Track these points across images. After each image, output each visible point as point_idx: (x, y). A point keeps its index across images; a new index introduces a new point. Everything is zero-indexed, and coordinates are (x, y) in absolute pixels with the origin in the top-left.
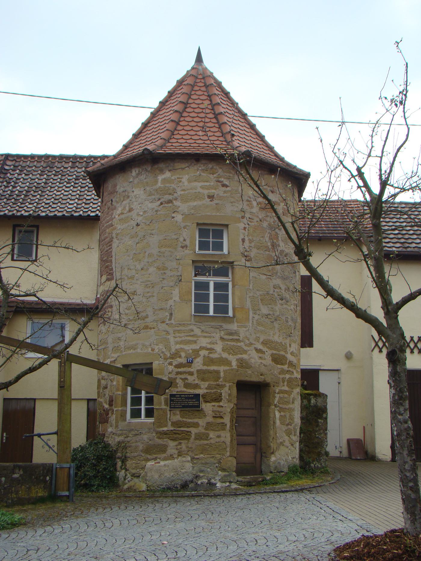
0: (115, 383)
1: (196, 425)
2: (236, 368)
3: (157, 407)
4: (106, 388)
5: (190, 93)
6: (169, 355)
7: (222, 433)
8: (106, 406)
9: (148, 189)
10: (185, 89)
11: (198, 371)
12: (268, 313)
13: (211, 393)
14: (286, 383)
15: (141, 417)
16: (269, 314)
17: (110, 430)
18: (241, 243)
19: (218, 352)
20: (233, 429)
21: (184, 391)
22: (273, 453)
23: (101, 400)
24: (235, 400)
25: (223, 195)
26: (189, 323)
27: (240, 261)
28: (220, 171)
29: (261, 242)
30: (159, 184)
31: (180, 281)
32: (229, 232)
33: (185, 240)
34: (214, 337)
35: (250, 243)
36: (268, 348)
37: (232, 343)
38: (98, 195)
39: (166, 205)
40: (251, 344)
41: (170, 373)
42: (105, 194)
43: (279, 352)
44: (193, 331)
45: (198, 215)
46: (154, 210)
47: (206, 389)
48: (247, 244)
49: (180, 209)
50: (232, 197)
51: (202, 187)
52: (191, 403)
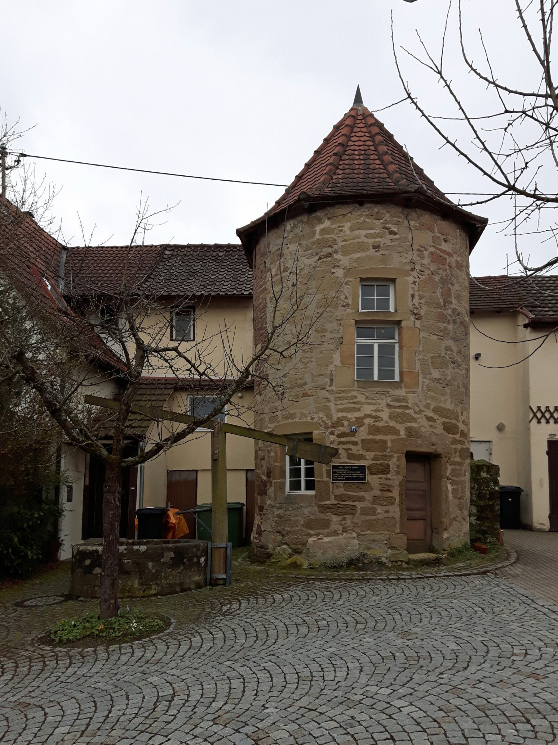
0: (272, 454)
1: (362, 499)
2: (405, 437)
3: (319, 479)
4: (263, 459)
5: (350, 135)
6: (330, 424)
7: (390, 508)
8: (264, 478)
9: (304, 242)
10: (344, 131)
11: (362, 440)
12: (439, 377)
13: (377, 464)
14: (458, 454)
15: (300, 490)
16: (440, 379)
17: (268, 502)
18: (410, 298)
19: (384, 420)
20: (402, 503)
21: (347, 463)
22: (446, 529)
23: (259, 472)
24: (404, 472)
25: (391, 244)
26: (353, 388)
27: (409, 319)
28: (388, 215)
29: (432, 299)
30: (317, 236)
31: (342, 343)
32: (397, 287)
33: (346, 298)
34: (379, 404)
35: (420, 299)
36: (440, 415)
37: (400, 411)
38: (251, 267)
39: (325, 260)
40: (421, 411)
41: (331, 443)
42: (257, 258)
43: (451, 419)
44: (356, 397)
45: (361, 268)
46: (311, 267)
47: (372, 460)
48: (416, 300)
49: (341, 262)
50: (400, 247)
51: (366, 236)
52: (355, 475)
